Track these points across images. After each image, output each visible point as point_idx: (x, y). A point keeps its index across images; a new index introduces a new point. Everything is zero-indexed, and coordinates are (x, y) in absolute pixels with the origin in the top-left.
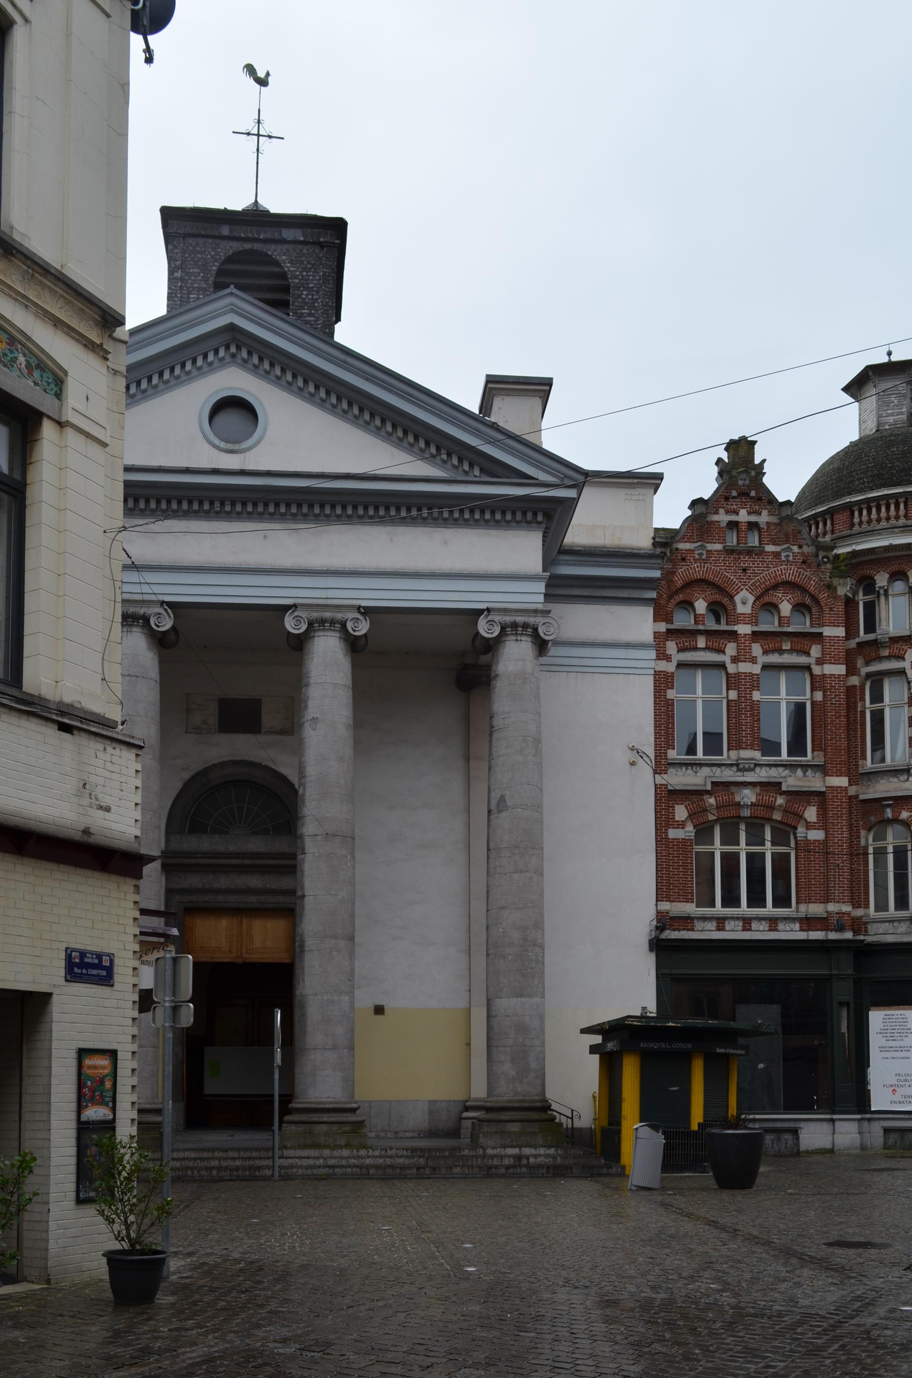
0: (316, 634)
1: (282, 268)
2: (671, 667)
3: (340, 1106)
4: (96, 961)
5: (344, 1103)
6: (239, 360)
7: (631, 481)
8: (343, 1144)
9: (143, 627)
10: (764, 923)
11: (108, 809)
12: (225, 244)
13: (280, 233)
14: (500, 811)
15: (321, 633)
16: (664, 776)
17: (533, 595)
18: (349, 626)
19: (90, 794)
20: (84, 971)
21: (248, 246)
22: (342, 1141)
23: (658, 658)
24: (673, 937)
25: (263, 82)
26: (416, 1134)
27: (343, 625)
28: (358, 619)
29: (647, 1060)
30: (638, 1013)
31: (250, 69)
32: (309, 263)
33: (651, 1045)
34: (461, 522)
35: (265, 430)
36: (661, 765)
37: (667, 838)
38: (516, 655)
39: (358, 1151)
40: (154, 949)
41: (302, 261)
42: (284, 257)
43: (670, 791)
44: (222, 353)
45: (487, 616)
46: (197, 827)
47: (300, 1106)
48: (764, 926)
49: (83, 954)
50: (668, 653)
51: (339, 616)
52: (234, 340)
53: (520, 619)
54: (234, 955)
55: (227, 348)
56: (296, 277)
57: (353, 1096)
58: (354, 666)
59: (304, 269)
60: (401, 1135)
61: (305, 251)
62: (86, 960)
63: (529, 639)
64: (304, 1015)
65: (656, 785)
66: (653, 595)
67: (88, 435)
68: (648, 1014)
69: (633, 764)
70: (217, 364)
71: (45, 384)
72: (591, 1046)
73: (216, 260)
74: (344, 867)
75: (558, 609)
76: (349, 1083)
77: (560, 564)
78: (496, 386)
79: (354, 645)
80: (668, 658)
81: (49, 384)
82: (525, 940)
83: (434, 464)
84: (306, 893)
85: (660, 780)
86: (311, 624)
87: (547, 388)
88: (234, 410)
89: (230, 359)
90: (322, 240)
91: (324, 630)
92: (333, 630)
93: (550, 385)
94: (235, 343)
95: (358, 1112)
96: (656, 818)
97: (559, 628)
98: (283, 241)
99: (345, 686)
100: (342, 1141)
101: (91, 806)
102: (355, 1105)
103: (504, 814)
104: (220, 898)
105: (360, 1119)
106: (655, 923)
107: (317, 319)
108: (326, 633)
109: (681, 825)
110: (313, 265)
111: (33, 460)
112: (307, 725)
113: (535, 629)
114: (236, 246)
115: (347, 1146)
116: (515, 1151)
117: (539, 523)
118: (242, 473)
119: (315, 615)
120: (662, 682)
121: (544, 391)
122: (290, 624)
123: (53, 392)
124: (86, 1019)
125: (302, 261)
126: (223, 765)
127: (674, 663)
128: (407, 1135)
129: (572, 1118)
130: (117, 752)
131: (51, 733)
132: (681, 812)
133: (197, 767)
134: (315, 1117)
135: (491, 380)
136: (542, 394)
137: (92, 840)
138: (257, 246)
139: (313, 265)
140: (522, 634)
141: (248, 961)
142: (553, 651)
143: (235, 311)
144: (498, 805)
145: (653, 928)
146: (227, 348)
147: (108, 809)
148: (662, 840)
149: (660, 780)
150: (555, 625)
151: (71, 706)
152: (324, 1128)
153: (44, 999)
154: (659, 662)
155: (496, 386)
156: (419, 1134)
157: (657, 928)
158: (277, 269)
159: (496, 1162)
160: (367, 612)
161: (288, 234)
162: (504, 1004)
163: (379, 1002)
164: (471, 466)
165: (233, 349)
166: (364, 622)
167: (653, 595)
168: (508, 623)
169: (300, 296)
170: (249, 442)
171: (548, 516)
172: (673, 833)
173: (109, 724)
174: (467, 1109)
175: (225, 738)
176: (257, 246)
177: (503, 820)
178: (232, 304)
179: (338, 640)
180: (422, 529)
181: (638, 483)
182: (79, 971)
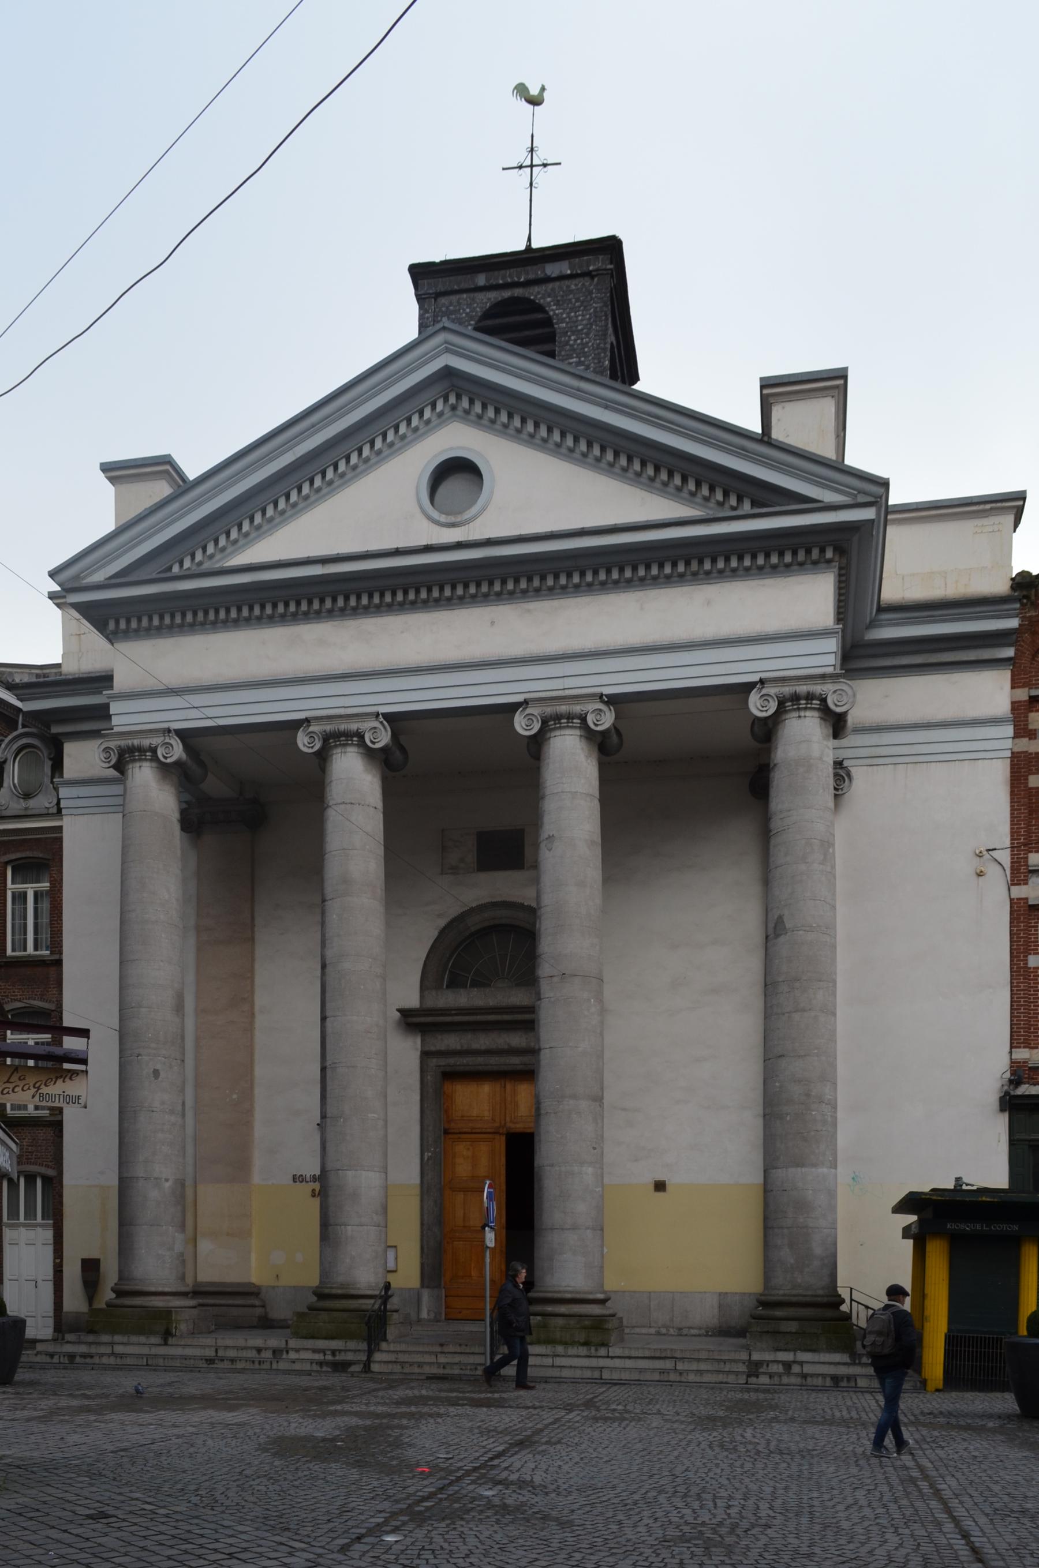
0: (553, 734)
1: (546, 312)
3: (578, 1296)
6: (460, 412)
7: (981, 507)
8: (582, 1341)
9: (358, 745)
12: (480, 296)
13: (544, 271)
14: (777, 936)
15: (557, 733)
16: (1024, 888)
17: (825, 654)
18: (590, 719)
21: (507, 294)
22: (581, 1337)
24: (1033, 1093)
25: (535, 101)
26: (703, 1332)
27: (583, 719)
28: (600, 710)
29: (958, 1245)
30: (950, 1185)
31: (521, 90)
32: (577, 300)
33: (962, 1226)
34: (728, 573)
35: (492, 493)
37: (1026, 968)
38: (804, 737)
39: (596, 1350)
40: (57, 1078)
41: (570, 300)
42: (549, 299)
43: (1031, 906)
44: (440, 406)
45: (761, 689)
47: (541, 1295)
50: (1031, 727)
51: (577, 709)
52: (453, 388)
53: (803, 689)
54: (497, 1125)
55: (446, 399)
56: (563, 321)
57: (602, 1286)
58: (602, 767)
59: (572, 310)
60: (685, 1332)
61: (573, 287)
63: (816, 714)
65: (1011, 900)
66: (1010, 652)
68: (964, 1187)
69: (980, 874)
70: (435, 421)
73: (472, 318)
74: (586, 1013)
77: (881, 626)
78: (775, 391)
79: (603, 745)
84: (542, 1046)
85: (1018, 892)
86: (545, 722)
87: (841, 382)
88: (457, 472)
89: (450, 414)
90: (591, 268)
91: (560, 728)
92: (572, 727)
93: (845, 378)
94: (454, 391)
95: (608, 1304)
96: (1011, 942)
97: (854, 695)
98: (548, 280)
99: (588, 795)
100: (581, 1337)
102: (601, 1296)
105: (611, 1312)
106: (1008, 1075)
108: (563, 732)
110: (582, 302)
112: (542, 846)
113: (824, 700)
114: (494, 296)
117: (829, 561)
118: (459, 546)
119: (549, 710)
121: (837, 387)
125: (570, 300)
126: (482, 908)
128: (693, 1332)
133: (454, 911)
134: (549, 1309)
135: (766, 384)
136: (835, 392)
138: (518, 292)
139: (582, 302)
140: (806, 709)
141: (513, 1131)
143: (449, 349)
144: (775, 928)
145: (1005, 1081)
146: (446, 399)
149: (1018, 892)
150: (850, 692)
152: (560, 1321)
154: (1017, 740)
155: (775, 391)
156: (707, 1332)
157: (1011, 1081)
158: (540, 316)
160: (612, 700)
161: (553, 269)
163: (660, 1177)
164: (740, 499)
165: (452, 400)
166: (608, 714)
167: (1010, 652)
168: (788, 696)
169: (567, 343)
170: (474, 510)
171: (841, 551)
175: (483, 876)
176: (518, 292)
178: (446, 342)
179: (578, 738)
180: (679, 589)
181: (991, 509)
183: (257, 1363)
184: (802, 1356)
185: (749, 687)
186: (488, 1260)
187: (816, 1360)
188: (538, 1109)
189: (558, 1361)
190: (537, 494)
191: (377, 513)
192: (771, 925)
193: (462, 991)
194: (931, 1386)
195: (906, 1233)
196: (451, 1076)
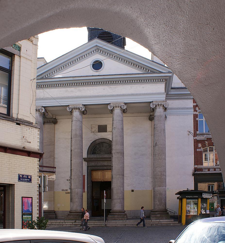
2: (197, 113)
4: (27, 177)
5: (121, 211)
10: (219, 169)
11: (30, 143)
14: (156, 146)
17: (163, 97)
19: (25, 139)
20: (23, 179)
23: (194, 111)
36: (195, 135)
38: (159, 111)
46: (94, 153)
47: (112, 211)
48: (219, 170)
49: (23, 175)
60: (137, 217)
62: (24, 177)
64: (113, 192)
67: (26, 59)
71: (16, 48)
72: (177, 197)
73: (98, 34)
75: (169, 102)
76: (123, 206)
80: (197, 111)
81: (17, 48)
82: (161, 174)
83: (140, 71)
94: (98, 49)
101: (25, 142)
102: (124, 211)
103: (157, 147)
104: (98, 168)
107: (119, 44)
109: (200, 148)
111: (13, 65)
115: (122, 220)
116: (159, 221)
120: (195, 116)
122: (109, 108)
123: (18, 50)
124: (21, 190)
127: (198, 112)
129: (175, 213)
130: (33, 129)
131: (14, 125)
132: (200, 145)
134: (115, 214)
137: (25, 149)
142: (168, 111)
147: (30, 143)
148: (195, 152)
151: (21, 119)
152: (117, 216)
153: (11, 186)
159: (154, 223)
162: (157, 188)
172: (198, 150)
173: (32, 123)
174: (152, 212)
177: (157, 148)
182: (22, 179)
183: (60, 225)
184: (161, 221)
185: (151, 102)
186: (105, 205)
187: (163, 221)
188: (112, 177)
189: (117, 223)
190: (111, 67)
191: (84, 68)
192: (155, 144)
193: (95, 155)
194: (183, 225)
195: (178, 198)
196: (92, 170)
